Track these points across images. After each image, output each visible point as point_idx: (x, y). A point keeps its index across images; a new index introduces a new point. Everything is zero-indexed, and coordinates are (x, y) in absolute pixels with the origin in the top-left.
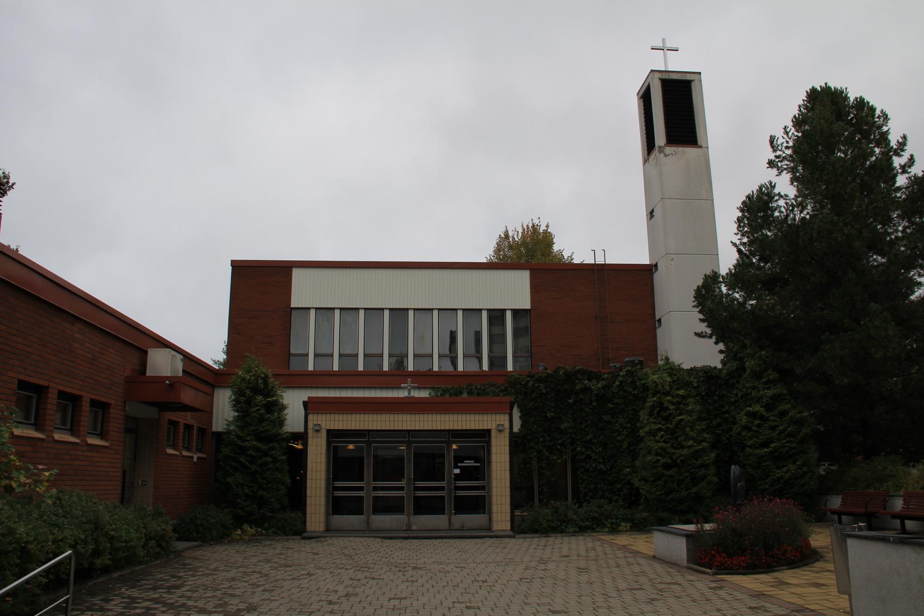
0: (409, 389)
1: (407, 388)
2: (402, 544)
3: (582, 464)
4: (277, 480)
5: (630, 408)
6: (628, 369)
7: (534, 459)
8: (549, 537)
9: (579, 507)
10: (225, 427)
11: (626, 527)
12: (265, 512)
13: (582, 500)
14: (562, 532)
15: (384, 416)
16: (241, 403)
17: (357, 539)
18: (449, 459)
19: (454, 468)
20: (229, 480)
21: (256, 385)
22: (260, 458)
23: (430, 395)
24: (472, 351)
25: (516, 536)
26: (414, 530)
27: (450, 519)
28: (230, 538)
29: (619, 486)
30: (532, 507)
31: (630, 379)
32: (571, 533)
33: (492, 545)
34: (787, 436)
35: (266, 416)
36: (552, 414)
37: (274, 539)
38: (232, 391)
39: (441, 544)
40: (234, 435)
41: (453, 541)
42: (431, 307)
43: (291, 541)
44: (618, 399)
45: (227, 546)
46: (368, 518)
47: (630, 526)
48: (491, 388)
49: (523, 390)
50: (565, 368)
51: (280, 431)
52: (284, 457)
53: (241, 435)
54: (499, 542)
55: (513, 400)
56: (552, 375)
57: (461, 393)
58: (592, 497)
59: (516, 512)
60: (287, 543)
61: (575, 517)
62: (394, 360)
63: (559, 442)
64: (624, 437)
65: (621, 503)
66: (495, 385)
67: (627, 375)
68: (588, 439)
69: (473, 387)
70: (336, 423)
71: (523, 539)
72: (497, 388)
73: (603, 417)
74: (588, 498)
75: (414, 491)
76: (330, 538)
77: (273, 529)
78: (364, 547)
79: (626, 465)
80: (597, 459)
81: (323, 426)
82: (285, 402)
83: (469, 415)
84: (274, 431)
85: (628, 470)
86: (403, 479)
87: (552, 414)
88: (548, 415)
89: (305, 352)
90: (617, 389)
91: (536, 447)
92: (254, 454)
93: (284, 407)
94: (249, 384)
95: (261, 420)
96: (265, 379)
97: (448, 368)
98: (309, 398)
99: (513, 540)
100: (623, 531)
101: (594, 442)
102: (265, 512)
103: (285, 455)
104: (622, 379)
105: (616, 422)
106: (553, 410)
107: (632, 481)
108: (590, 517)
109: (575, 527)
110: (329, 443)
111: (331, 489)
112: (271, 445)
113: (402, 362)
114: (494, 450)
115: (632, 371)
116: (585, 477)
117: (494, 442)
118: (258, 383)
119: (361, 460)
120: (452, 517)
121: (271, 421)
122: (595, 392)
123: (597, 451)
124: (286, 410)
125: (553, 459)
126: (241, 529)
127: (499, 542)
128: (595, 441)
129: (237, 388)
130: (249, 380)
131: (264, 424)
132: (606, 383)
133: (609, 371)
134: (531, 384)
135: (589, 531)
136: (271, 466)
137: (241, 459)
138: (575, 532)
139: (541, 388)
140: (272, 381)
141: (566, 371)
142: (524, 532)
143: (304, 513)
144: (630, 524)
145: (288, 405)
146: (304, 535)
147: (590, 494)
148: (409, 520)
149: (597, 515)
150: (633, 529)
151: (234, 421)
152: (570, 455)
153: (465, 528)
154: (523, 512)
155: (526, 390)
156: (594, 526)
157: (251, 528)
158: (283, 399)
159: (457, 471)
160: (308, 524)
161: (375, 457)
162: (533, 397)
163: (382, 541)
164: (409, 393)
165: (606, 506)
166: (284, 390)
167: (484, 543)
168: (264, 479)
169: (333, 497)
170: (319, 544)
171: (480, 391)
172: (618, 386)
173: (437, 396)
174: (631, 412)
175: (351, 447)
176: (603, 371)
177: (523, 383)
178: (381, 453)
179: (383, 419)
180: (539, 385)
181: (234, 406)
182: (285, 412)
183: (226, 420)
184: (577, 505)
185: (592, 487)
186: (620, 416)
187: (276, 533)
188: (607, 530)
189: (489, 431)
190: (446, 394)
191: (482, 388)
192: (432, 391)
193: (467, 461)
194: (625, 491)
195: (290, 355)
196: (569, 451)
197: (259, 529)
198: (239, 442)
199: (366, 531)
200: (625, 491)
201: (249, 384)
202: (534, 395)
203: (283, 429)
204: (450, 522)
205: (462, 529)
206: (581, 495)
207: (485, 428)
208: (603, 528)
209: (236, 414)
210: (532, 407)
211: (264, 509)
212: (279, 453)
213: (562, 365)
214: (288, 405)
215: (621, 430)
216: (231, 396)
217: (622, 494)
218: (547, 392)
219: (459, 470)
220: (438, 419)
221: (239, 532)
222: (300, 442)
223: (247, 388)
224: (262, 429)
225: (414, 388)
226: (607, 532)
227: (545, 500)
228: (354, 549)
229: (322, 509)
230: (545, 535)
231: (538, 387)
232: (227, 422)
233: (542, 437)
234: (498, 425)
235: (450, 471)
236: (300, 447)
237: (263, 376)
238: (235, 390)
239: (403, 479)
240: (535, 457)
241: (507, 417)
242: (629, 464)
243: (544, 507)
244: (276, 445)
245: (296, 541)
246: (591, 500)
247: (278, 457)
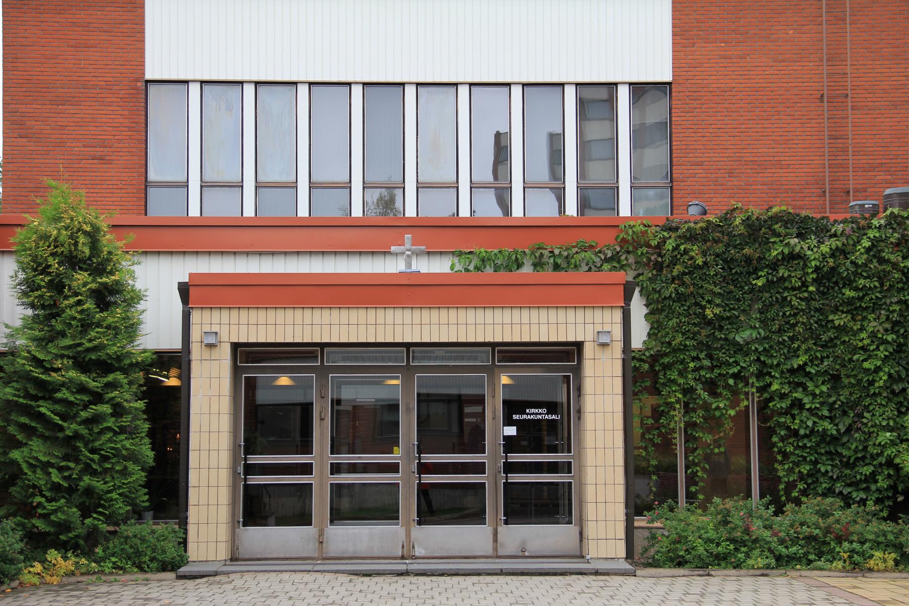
0: (408, 256)
1: (403, 253)
2: (394, 586)
3: (782, 420)
4: (124, 452)
5: (895, 300)
6: (892, 213)
7: (678, 406)
8: (709, 575)
9: (776, 514)
10: (5, 341)
11: (885, 561)
12: (96, 522)
13: (783, 498)
14: (737, 566)
15: (353, 313)
16: (39, 288)
17: (297, 577)
18: (494, 408)
20: (15, 455)
21: (73, 248)
22: (85, 407)
23: (452, 268)
24: (542, 173)
25: (638, 572)
26: (417, 558)
27: (495, 534)
28: (15, 584)
29: (867, 470)
30: (671, 510)
31: (896, 235)
32: (758, 568)
33: (586, 590)
35: (97, 316)
36: (717, 311)
37: (116, 580)
38: (18, 262)
39: (477, 587)
40: (25, 358)
41: (503, 579)
42: (453, 80)
43: (154, 584)
44: (865, 278)
45: (9, 600)
46: (321, 533)
47: (895, 560)
48: (583, 254)
49: (653, 258)
50: (747, 211)
51: (129, 348)
52: (140, 405)
53: (41, 356)
54: (602, 584)
55: (630, 279)
56: (719, 226)
57: (519, 266)
58: (804, 493)
59: (638, 520)
60: (143, 589)
61: (767, 534)
62: (374, 195)
63: (731, 372)
64: (879, 363)
65: (871, 506)
66: (591, 247)
67: (889, 224)
68: (795, 366)
69: (546, 253)
70: (253, 329)
71: (653, 580)
72: (596, 254)
73: (831, 317)
74: (795, 494)
75: (420, 473)
76: (238, 575)
77: (114, 559)
78: (312, 594)
79: (884, 423)
80: (816, 408)
81: (224, 336)
82: (139, 285)
83: (300, 311)
84: (116, 349)
85: (888, 434)
86: (395, 448)
87: (717, 311)
88: (708, 312)
90: (865, 256)
91: (681, 381)
92: (72, 399)
93: (135, 298)
94: (56, 247)
95: (86, 326)
96: (93, 236)
97: (489, 209)
98: (190, 275)
99: (631, 580)
100: (878, 571)
101: (810, 372)
102: (96, 522)
103: (141, 400)
104: (877, 235)
105: (862, 329)
106: (718, 301)
107: (897, 461)
108: (801, 536)
109: (767, 558)
110: (236, 371)
111: (241, 469)
112: (110, 378)
113: (392, 200)
114: (589, 385)
115: (902, 217)
116: (789, 449)
117: (588, 368)
118: (76, 244)
119: (306, 409)
120: (500, 529)
121: (108, 327)
122: (813, 263)
123: (817, 392)
124: (142, 302)
125: (718, 408)
126: (43, 561)
127: (602, 584)
128: (813, 371)
129: (30, 255)
130: (56, 240)
131: (93, 334)
132: (839, 244)
133: (848, 216)
134: (670, 245)
135: (798, 567)
136: (110, 423)
137: (43, 410)
138: (768, 567)
139: (692, 254)
140: (109, 241)
141: (748, 218)
142: (654, 564)
143: (184, 523)
144: (893, 555)
145: (146, 291)
146: (183, 570)
147: (801, 486)
148: (408, 534)
149: (817, 531)
150: (901, 567)
151: (25, 327)
152: (756, 399)
153: (527, 554)
154: (652, 521)
155: (660, 259)
156: (812, 557)
157: (65, 558)
158: (134, 278)
159: (511, 431)
160: (191, 546)
161: (337, 402)
162: (675, 273)
163: (350, 581)
164: (409, 265)
165: (838, 514)
166: (136, 259)
167: (570, 585)
168: (93, 451)
169: (246, 486)
170: (215, 588)
171: (559, 261)
172: (868, 250)
173: (467, 270)
174: (897, 308)
175: (284, 380)
176: (833, 217)
177: (654, 243)
178: (348, 393)
179: (353, 320)
180: (689, 246)
181: (25, 294)
182: (139, 306)
183: (7, 326)
184: (772, 509)
185: (805, 469)
186: (871, 317)
187: (121, 568)
188: (840, 567)
189: (579, 345)
190: (488, 267)
191: (565, 254)
192: (456, 260)
193: (533, 411)
194: (882, 483)
195: (147, 184)
196: (755, 390)
197: (84, 561)
198: (37, 373)
199: (317, 559)
200: (882, 483)
201: (56, 247)
202: (678, 269)
203: (138, 342)
204: (495, 540)
205: (521, 556)
206: (782, 486)
207: (571, 339)
208: (832, 562)
209: (30, 312)
210: (673, 295)
211: (95, 515)
212: (127, 396)
213: (739, 205)
214: (146, 291)
215: (872, 348)
216: (16, 272)
217: (873, 487)
218: (705, 263)
219: (515, 428)
220: (471, 320)
221: (38, 567)
222: (174, 372)
223: (53, 255)
224: (88, 345)
225: (418, 254)
226: (840, 571)
227: (701, 497)
228: (290, 598)
229: (224, 514)
230: (701, 572)
231: (686, 252)
232: (8, 331)
233: (694, 359)
234: (598, 332)
235: (496, 432)
236: (173, 382)
237: (88, 228)
238: (26, 260)
239: (395, 448)
240: (678, 401)
241: (618, 315)
242: (891, 423)
243: (699, 511)
244: (119, 376)
245: (164, 583)
246: (804, 499)
247: (125, 404)
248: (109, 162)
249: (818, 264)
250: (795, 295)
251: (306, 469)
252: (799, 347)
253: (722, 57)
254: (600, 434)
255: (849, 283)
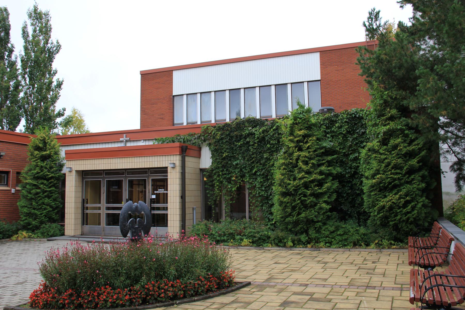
19: (152, 194)
34: (392, 168)
89: (225, 118)
159: (154, 197)
193: (160, 190)
207: (164, 166)
235: (149, 196)
248: (164, 119)
249: (258, 136)
250: (252, 148)
251: (108, 208)
252: (254, 165)
253: (336, 70)
254: (172, 197)
255: (269, 142)
